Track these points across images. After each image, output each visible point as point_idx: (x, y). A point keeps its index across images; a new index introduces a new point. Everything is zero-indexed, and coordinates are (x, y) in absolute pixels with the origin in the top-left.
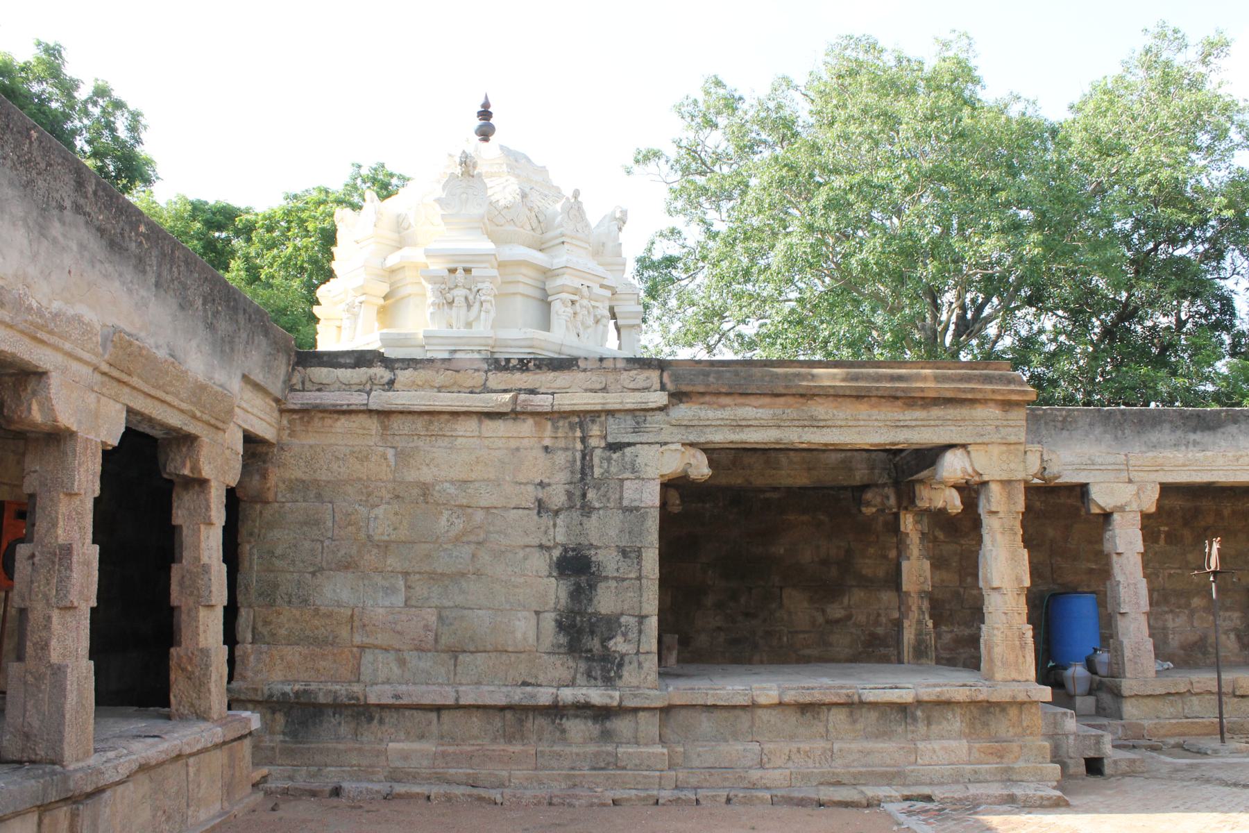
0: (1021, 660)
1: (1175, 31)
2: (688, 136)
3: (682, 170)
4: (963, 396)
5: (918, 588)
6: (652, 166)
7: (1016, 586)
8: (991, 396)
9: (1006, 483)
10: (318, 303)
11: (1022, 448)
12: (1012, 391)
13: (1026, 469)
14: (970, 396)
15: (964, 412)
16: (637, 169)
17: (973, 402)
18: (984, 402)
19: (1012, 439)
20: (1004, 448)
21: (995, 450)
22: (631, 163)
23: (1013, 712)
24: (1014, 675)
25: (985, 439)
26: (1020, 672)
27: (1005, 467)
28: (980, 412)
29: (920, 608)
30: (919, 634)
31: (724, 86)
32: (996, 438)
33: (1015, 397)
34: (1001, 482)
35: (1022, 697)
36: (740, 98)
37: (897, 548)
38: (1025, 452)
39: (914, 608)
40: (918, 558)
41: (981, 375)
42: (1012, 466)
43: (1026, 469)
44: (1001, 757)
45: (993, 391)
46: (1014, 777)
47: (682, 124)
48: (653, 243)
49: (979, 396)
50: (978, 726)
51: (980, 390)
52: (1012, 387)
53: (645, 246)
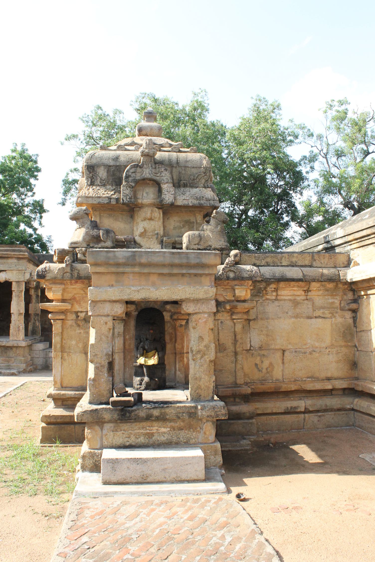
0: (18, 334)
1: (264, 99)
2: (88, 130)
3: (86, 143)
4: (4, 256)
5: (34, 313)
6: (72, 141)
7: (18, 312)
8: (13, 256)
9: (18, 282)
10: (35, 177)
11: (24, 272)
12: (20, 255)
13: (24, 278)
14: (6, 256)
15: (5, 261)
16: (66, 142)
17: (8, 258)
18: (11, 258)
19: (20, 269)
20: (18, 271)
21: (15, 272)
22: (63, 140)
23: (14, 349)
24: (15, 339)
25: (12, 269)
26: (17, 338)
27: (17, 277)
28: (10, 261)
29: (34, 319)
30: (34, 327)
31: (101, 110)
32: (15, 268)
33: (21, 256)
34: (16, 282)
35: (15, 345)
36: (108, 115)
37: (262, 280)
38: (25, 273)
39: (32, 319)
40: (35, 303)
41: (12, 249)
42: (20, 277)
43: (24, 278)
44: (9, 362)
45: (14, 255)
46: (11, 368)
47: (84, 125)
48: (68, 174)
49: (9, 256)
50: (4, 353)
51: (10, 254)
52: (21, 253)
53: (65, 175)
